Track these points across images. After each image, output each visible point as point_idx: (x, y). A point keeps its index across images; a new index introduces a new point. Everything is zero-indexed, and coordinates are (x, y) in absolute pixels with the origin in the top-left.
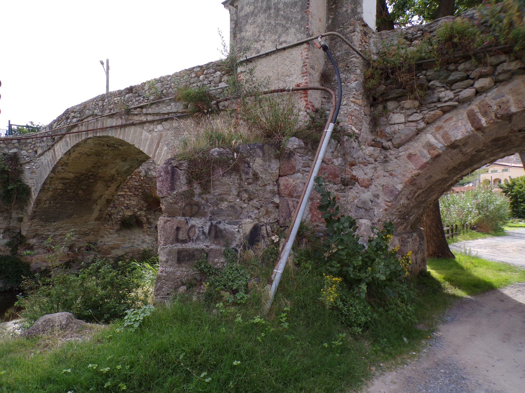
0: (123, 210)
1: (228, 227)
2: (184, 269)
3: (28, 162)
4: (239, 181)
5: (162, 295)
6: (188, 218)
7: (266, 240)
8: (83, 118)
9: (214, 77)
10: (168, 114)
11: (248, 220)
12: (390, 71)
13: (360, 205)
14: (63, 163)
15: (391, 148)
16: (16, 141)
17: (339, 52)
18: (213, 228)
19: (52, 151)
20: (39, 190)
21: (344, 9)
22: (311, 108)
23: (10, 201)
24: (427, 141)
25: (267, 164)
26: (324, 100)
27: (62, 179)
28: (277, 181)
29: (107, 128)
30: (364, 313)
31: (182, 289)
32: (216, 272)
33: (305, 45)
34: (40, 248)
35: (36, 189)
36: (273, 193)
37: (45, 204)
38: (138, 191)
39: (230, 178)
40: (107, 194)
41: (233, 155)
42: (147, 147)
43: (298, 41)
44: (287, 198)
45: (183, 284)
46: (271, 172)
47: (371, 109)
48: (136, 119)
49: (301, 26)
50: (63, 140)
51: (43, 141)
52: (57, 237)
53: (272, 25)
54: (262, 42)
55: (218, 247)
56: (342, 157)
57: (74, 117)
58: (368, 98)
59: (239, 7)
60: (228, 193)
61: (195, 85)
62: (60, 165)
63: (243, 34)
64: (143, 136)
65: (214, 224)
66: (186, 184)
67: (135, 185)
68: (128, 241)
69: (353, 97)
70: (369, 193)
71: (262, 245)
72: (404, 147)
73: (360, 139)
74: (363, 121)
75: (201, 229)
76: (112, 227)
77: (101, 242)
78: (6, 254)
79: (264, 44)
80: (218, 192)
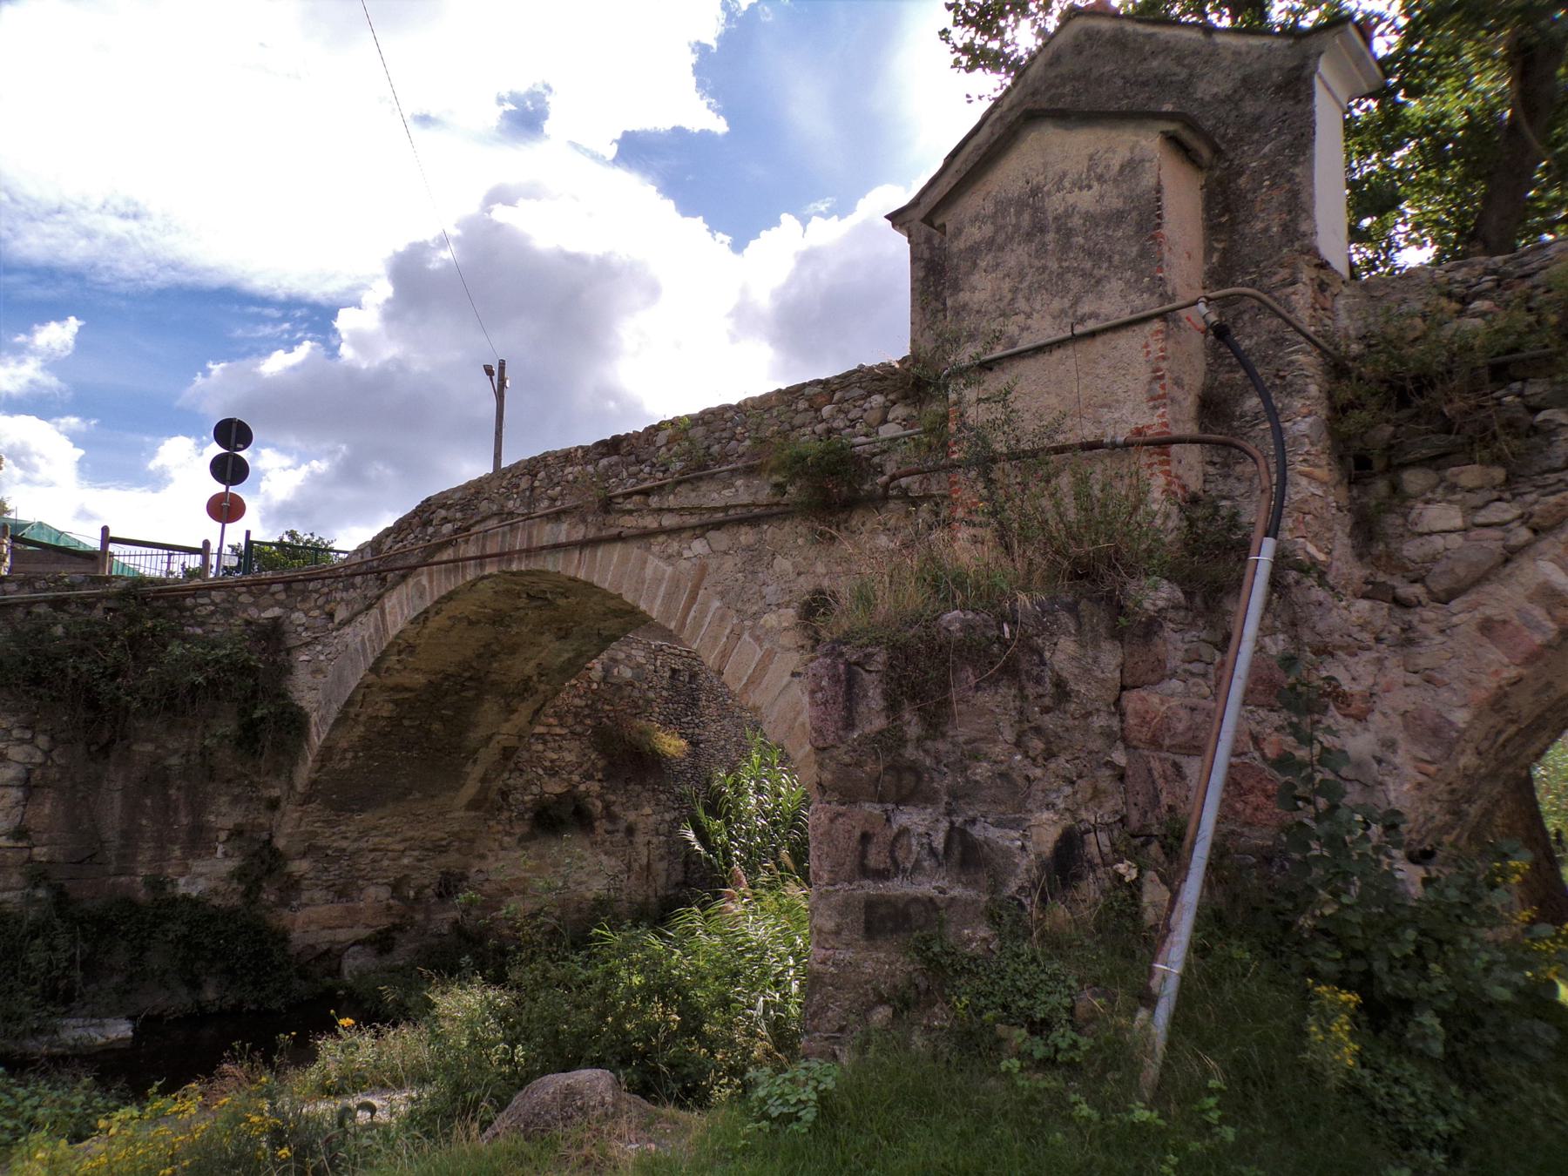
0: (539, 777)
1: (994, 833)
2: (882, 955)
3: (307, 644)
4: (1018, 703)
5: (827, 1031)
6: (890, 806)
7: (1100, 872)
8: (472, 522)
9: (865, 410)
10: (726, 508)
11: (1047, 815)
12: (1410, 387)
14: (404, 645)
15: (1424, 603)
16: (279, 587)
17: (1251, 337)
18: (957, 838)
19: (375, 611)
20: (331, 721)
21: (1259, 226)
22: (1180, 492)
23: (256, 752)
24: (1541, 579)
25: (1090, 653)
26: (1211, 469)
27: (397, 688)
28: (1118, 700)
29: (543, 548)
30: (1438, 1106)
31: (881, 1014)
32: (973, 966)
33: (1157, 325)
34: (317, 885)
35: (323, 719)
36: (1108, 734)
37: (343, 759)
38: (581, 722)
39: (996, 693)
40: (506, 731)
41: (1001, 629)
42: (659, 601)
43: (1132, 313)
44: (1146, 753)
45: (882, 1000)
46: (1102, 676)
47: (1350, 491)
48: (629, 523)
49: (1142, 274)
50: (411, 581)
51: (353, 586)
52: (362, 856)
53: (1052, 273)
54: (1023, 316)
55: (971, 894)
56: (1286, 632)
57: (446, 520)
58: (1341, 458)
59: (950, 228)
60: (992, 736)
61: (808, 430)
62: (395, 649)
63: (964, 297)
64: (649, 572)
65: (957, 825)
66: (883, 710)
67: (576, 707)
68: (552, 869)
69: (1305, 460)
70: (1369, 737)
71: (1090, 889)
72: (1463, 598)
73: (1330, 579)
74: (1336, 527)
75: (925, 841)
76: (508, 828)
77: (480, 871)
78: (230, 903)
79: (1029, 321)
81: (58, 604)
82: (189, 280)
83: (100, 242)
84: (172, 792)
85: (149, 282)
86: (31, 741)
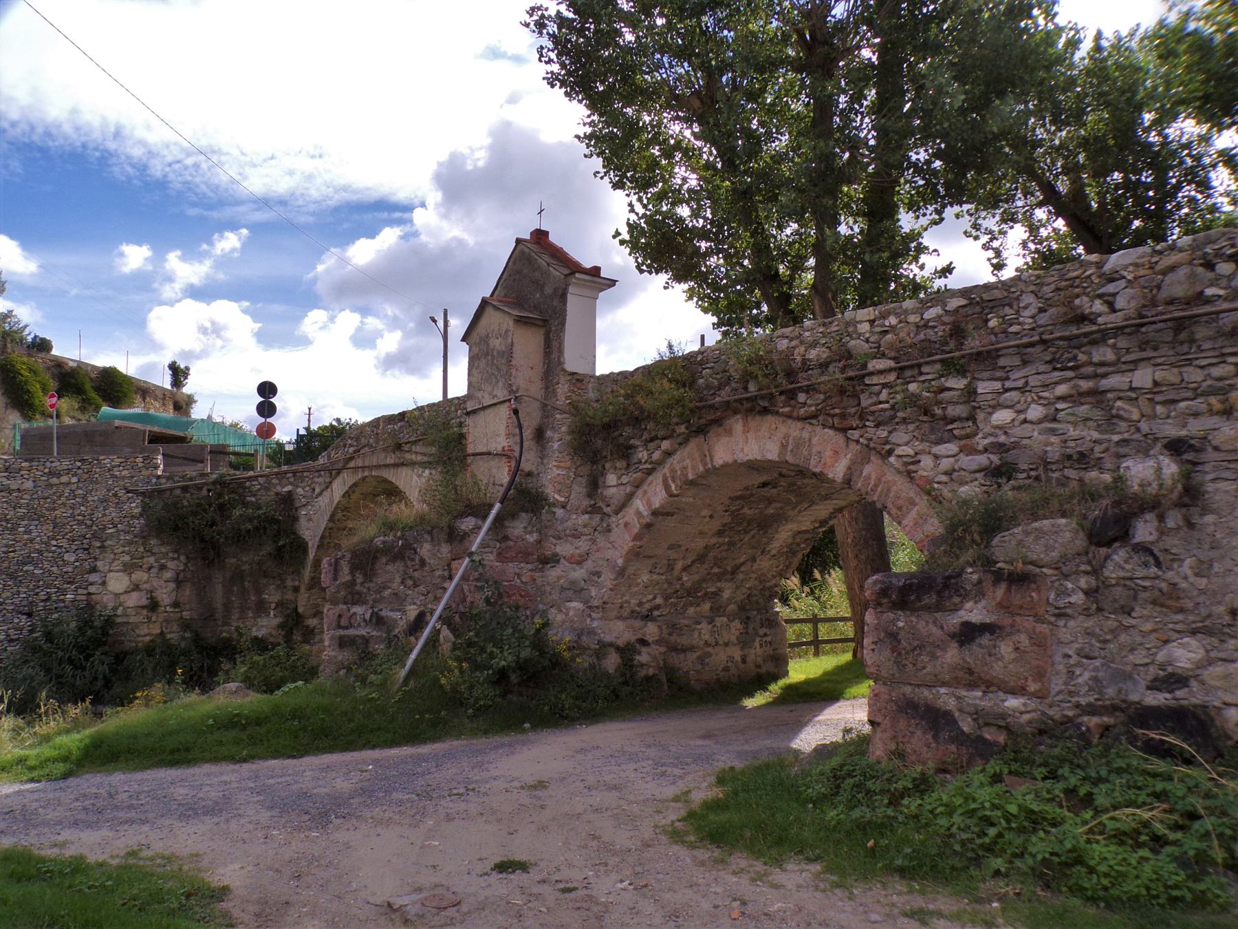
3: (305, 505)
11: (412, 607)
13: (565, 585)
16: (291, 475)
19: (329, 490)
28: (449, 565)
31: (342, 672)
45: (344, 668)
50: (341, 475)
55: (379, 634)
57: (351, 446)
60: (391, 581)
80: (380, 580)
81: (185, 489)
82: (354, 198)
83: (297, 177)
84: (246, 583)
85: (329, 203)
86: (178, 558)
